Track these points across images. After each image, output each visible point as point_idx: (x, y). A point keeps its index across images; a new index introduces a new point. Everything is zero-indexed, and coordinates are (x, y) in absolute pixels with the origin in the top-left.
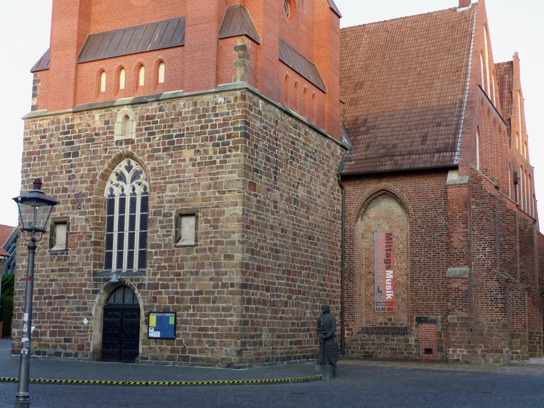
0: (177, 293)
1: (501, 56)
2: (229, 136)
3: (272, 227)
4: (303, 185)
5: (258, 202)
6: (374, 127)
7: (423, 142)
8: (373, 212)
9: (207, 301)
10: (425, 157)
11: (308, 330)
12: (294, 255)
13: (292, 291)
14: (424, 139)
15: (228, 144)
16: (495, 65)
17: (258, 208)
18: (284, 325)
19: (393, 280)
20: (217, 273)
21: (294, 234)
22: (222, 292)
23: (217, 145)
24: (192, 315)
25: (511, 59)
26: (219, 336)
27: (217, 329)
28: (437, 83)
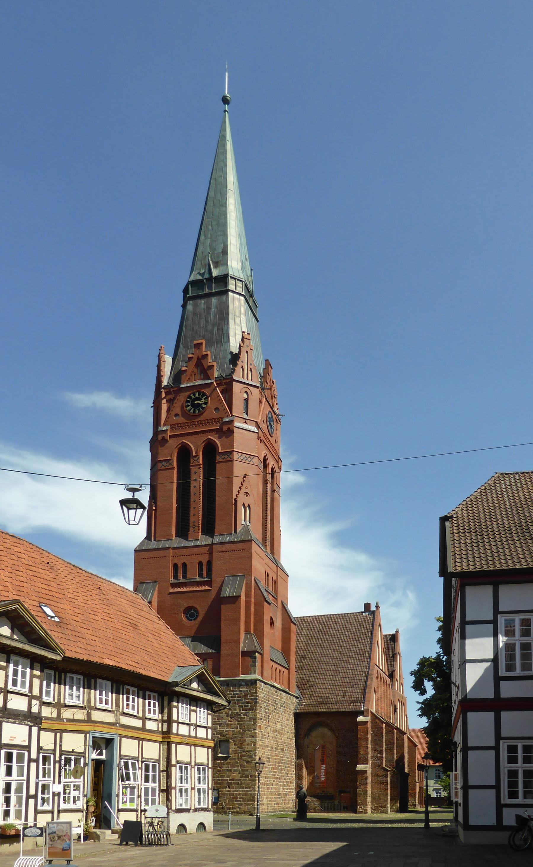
0: (219, 780)
1: (389, 631)
2: (248, 703)
3: (267, 746)
4: (279, 722)
5: (262, 734)
6: (314, 685)
7: (344, 696)
8: (314, 734)
9: (237, 784)
10: (346, 705)
11: (281, 797)
12: (276, 759)
13: (275, 778)
14: (345, 694)
15: (248, 706)
16: (384, 636)
17: (262, 737)
18: (272, 795)
19: (326, 770)
20: (242, 770)
21: (276, 748)
22: (245, 780)
23: (242, 706)
24: (229, 791)
25: (395, 633)
26: (244, 801)
27: (242, 798)
28: (351, 661)
